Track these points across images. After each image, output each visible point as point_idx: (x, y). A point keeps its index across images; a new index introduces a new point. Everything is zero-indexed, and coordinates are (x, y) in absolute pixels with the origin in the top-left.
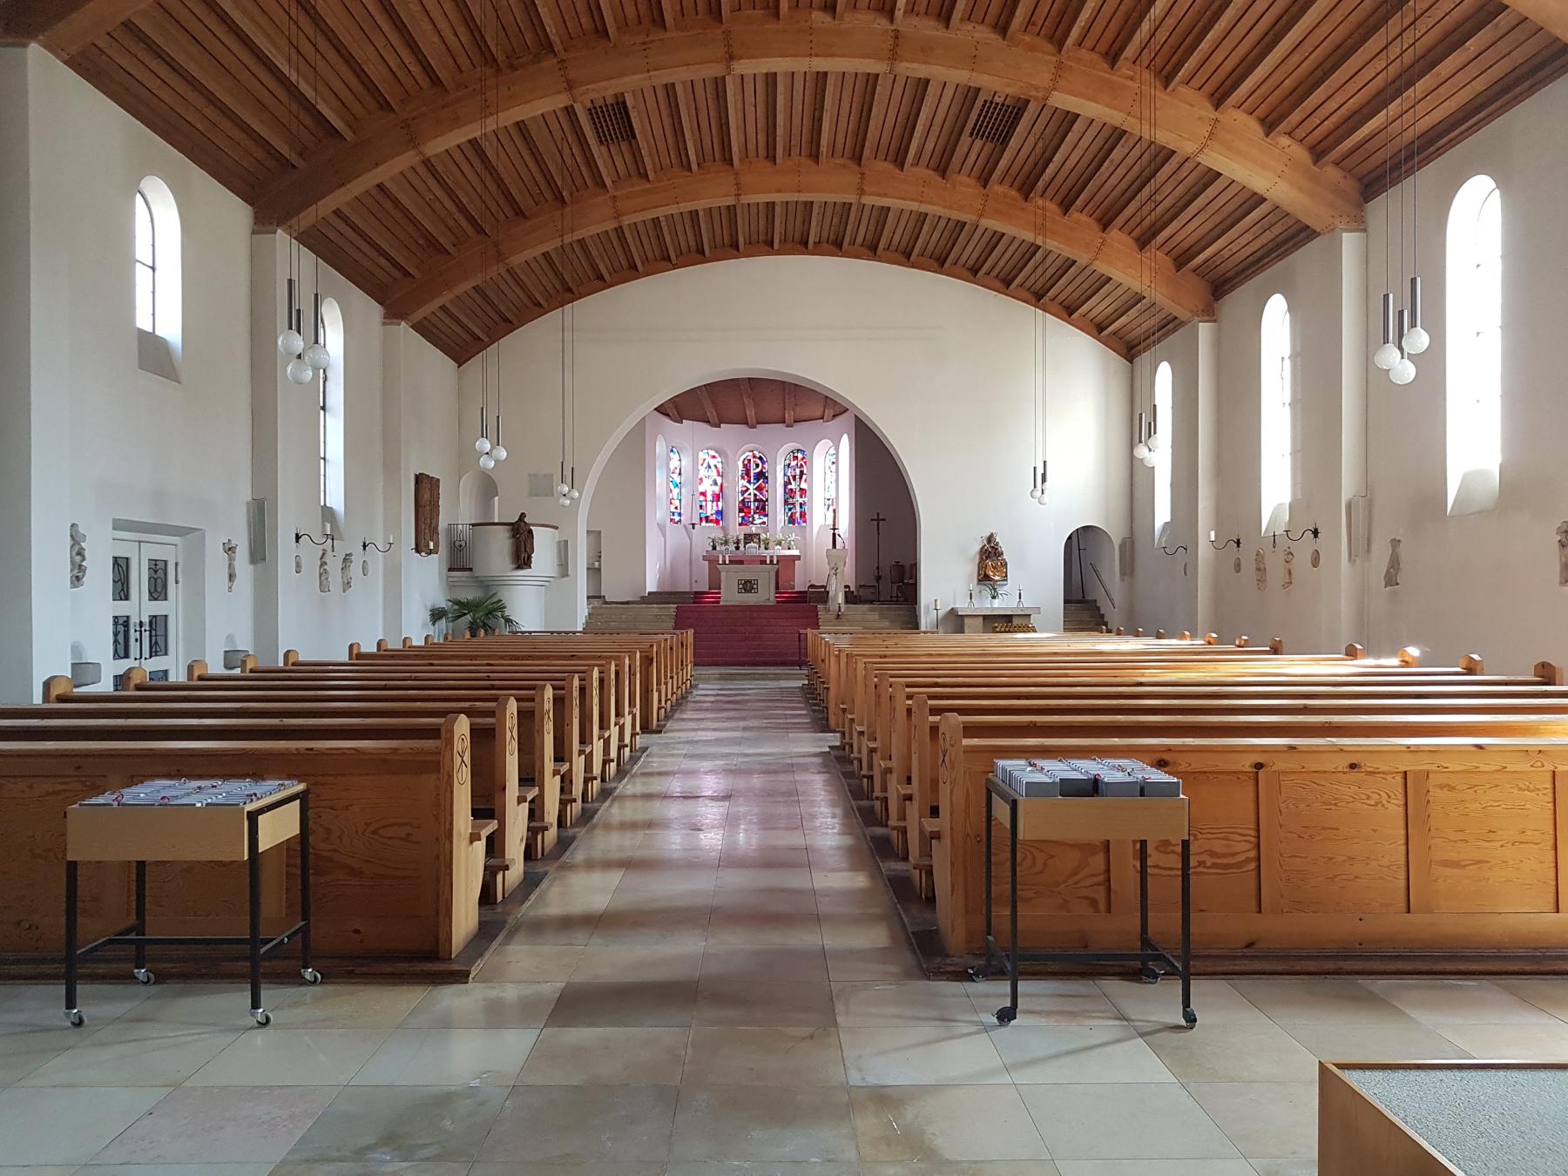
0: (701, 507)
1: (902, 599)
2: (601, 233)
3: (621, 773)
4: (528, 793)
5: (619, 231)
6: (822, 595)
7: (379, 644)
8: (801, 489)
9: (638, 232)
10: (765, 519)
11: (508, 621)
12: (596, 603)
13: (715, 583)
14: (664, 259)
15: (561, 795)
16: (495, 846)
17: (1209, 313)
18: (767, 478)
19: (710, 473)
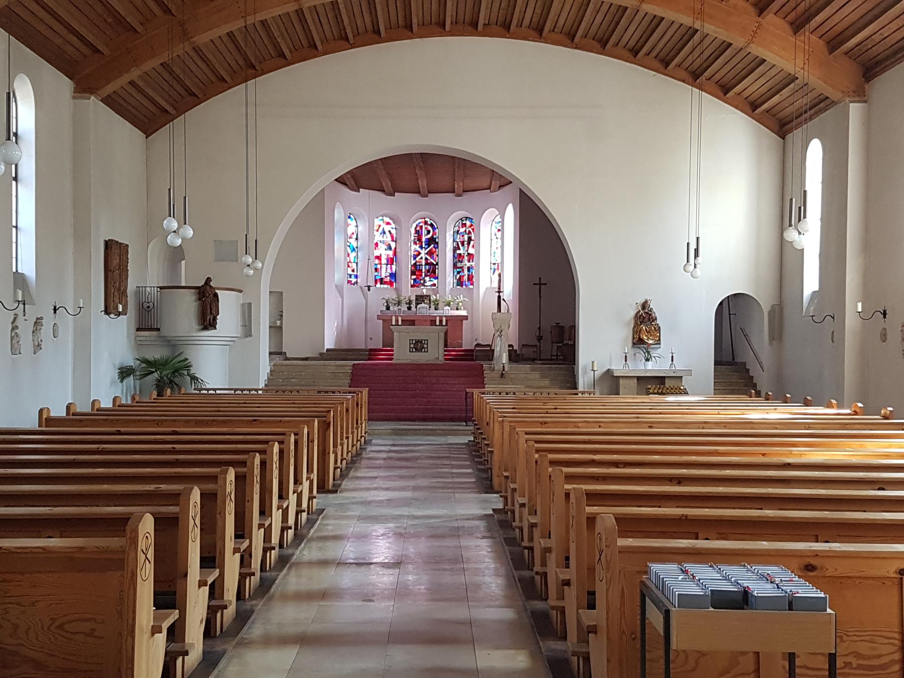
0: (376, 270)
1: (562, 357)
2: (283, 14)
3: (299, 538)
4: (208, 577)
5: (299, 12)
6: (488, 353)
7: (68, 408)
8: (469, 254)
9: (317, 13)
10: (435, 281)
11: (194, 378)
12: (278, 360)
13: (388, 342)
14: (341, 38)
15: (241, 568)
16: (176, 633)
17: (860, 94)
18: (437, 243)
19: (385, 239)
